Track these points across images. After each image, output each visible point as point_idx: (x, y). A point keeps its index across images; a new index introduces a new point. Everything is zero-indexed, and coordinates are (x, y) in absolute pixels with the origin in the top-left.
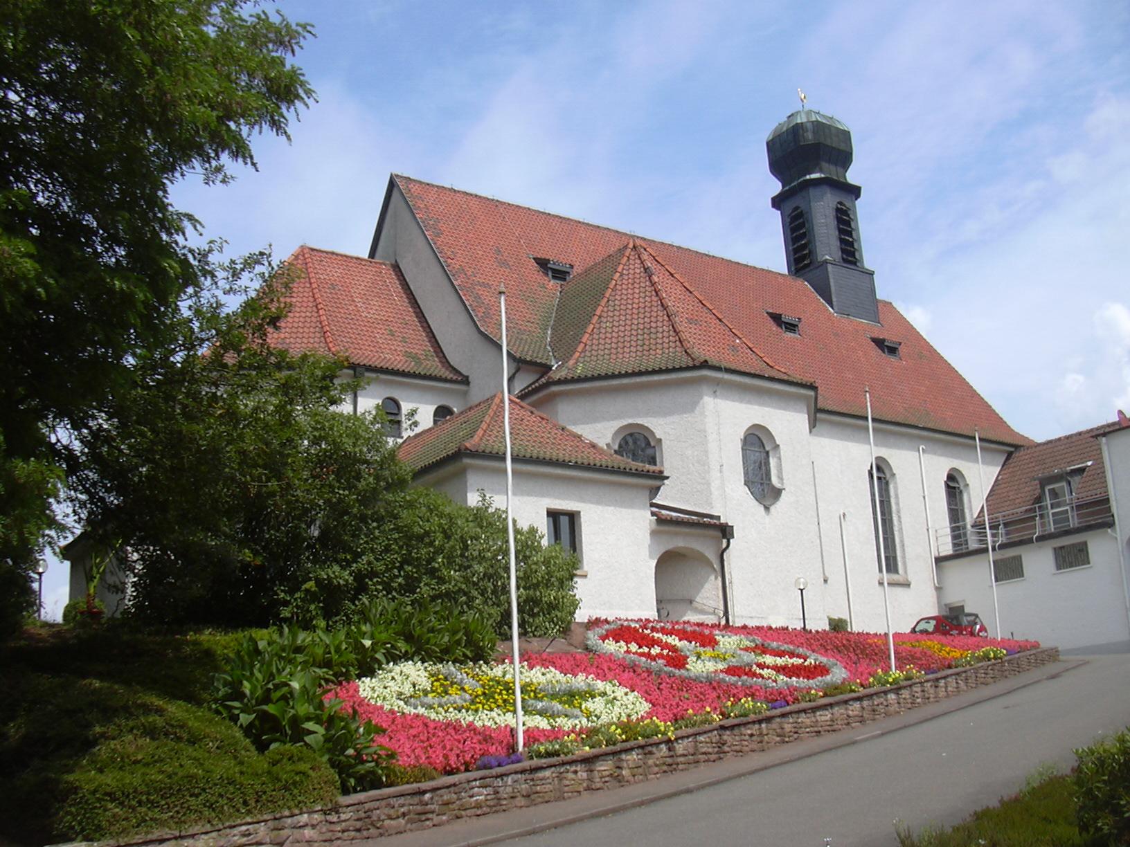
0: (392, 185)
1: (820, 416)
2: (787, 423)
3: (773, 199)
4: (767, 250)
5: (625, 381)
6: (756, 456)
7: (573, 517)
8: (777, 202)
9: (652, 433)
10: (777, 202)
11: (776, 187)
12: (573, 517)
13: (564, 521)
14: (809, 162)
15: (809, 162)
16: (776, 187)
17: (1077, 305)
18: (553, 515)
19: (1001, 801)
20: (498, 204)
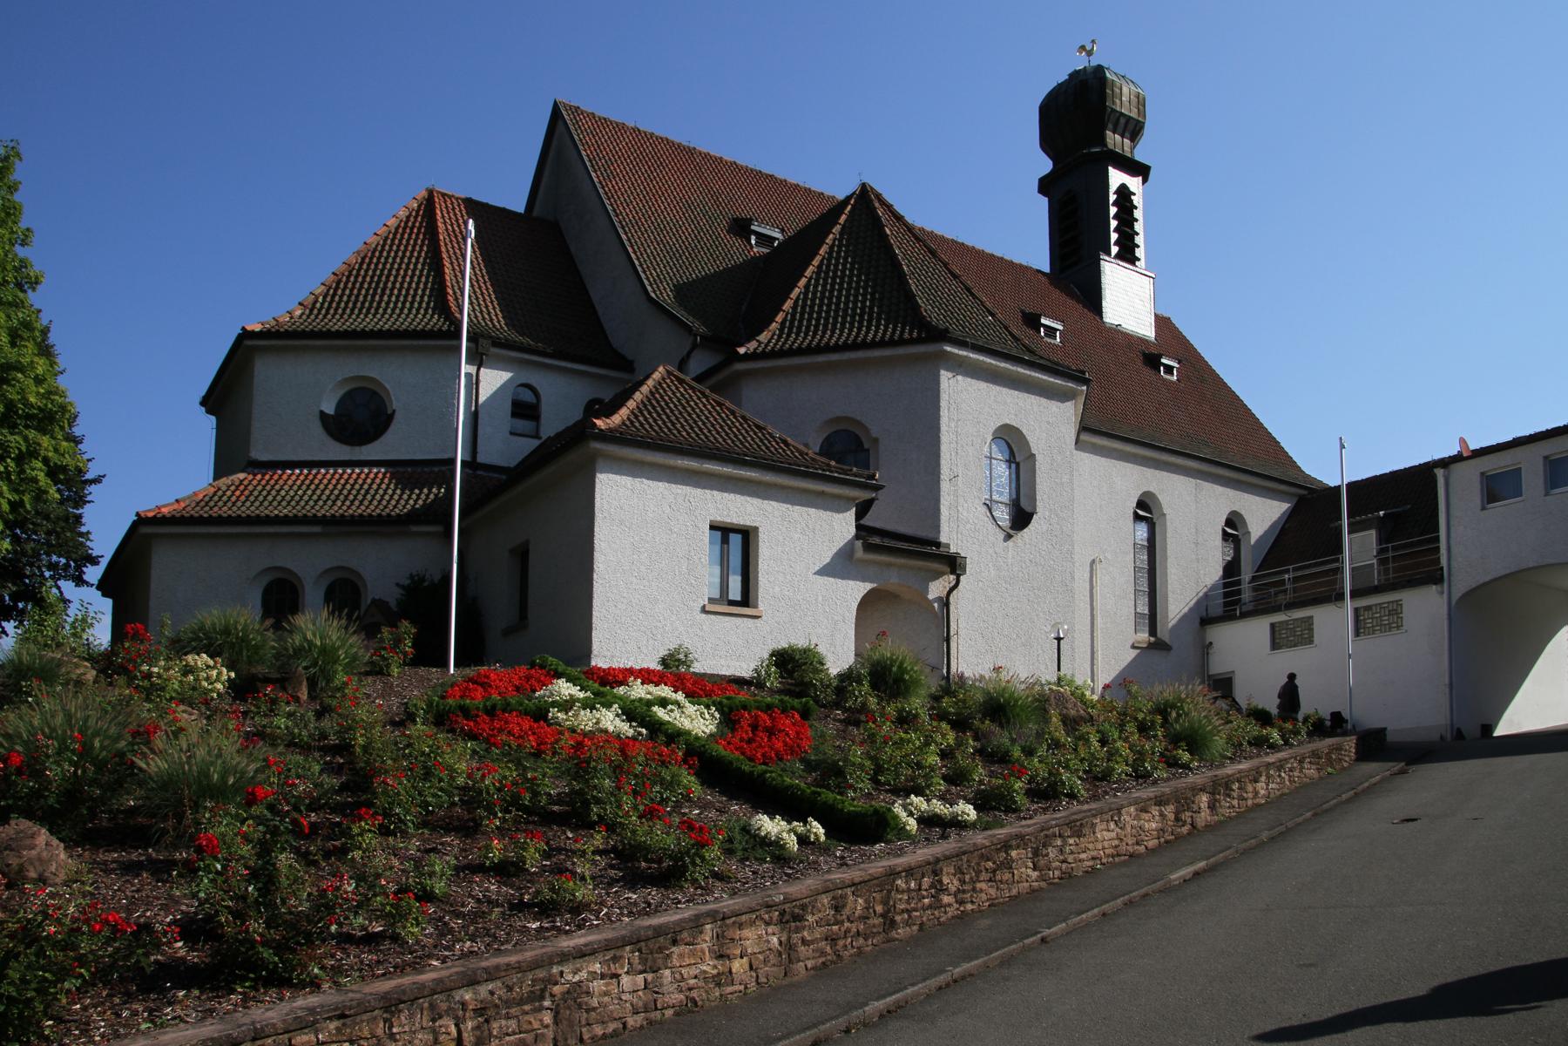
0: (556, 114)
1: (1096, 430)
2: (1050, 422)
3: (1042, 181)
4: (1038, 256)
5: (835, 357)
6: (1024, 504)
7: (748, 535)
8: (1045, 186)
9: (867, 430)
10: (1045, 186)
11: (1045, 165)
12: (748, 535)
13: (736, 540)
14: (1083, 128)
15: (1083, 128)
16: (1045, 165)
17: (1471, 265)
18: (723, 531)
19: (412, 577)
20: (691, 152)
